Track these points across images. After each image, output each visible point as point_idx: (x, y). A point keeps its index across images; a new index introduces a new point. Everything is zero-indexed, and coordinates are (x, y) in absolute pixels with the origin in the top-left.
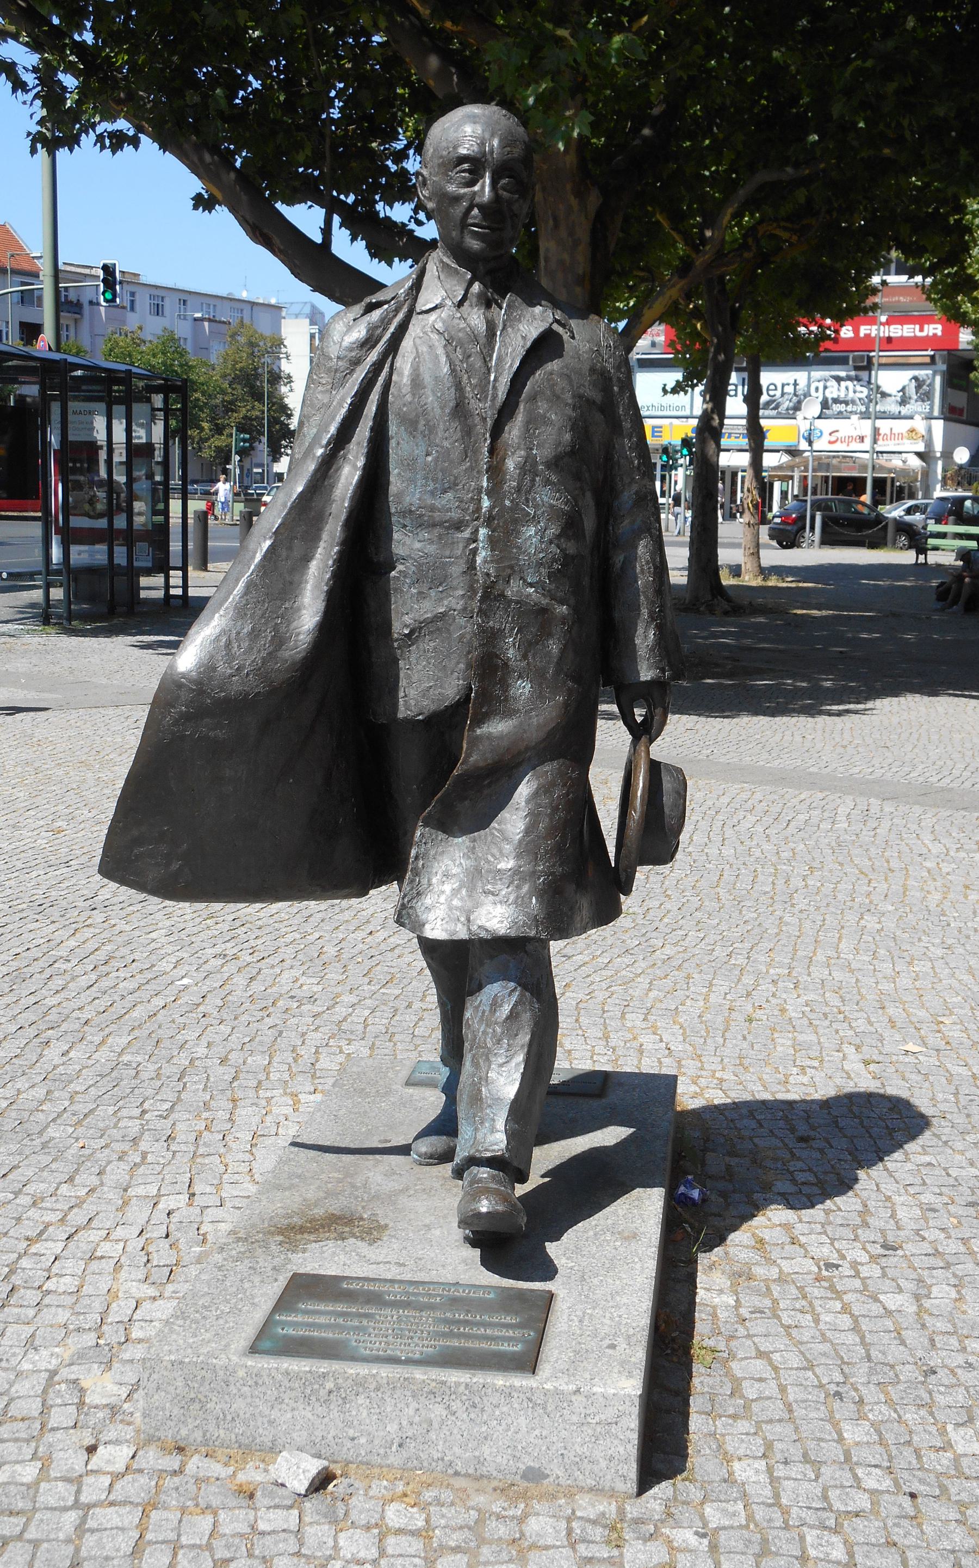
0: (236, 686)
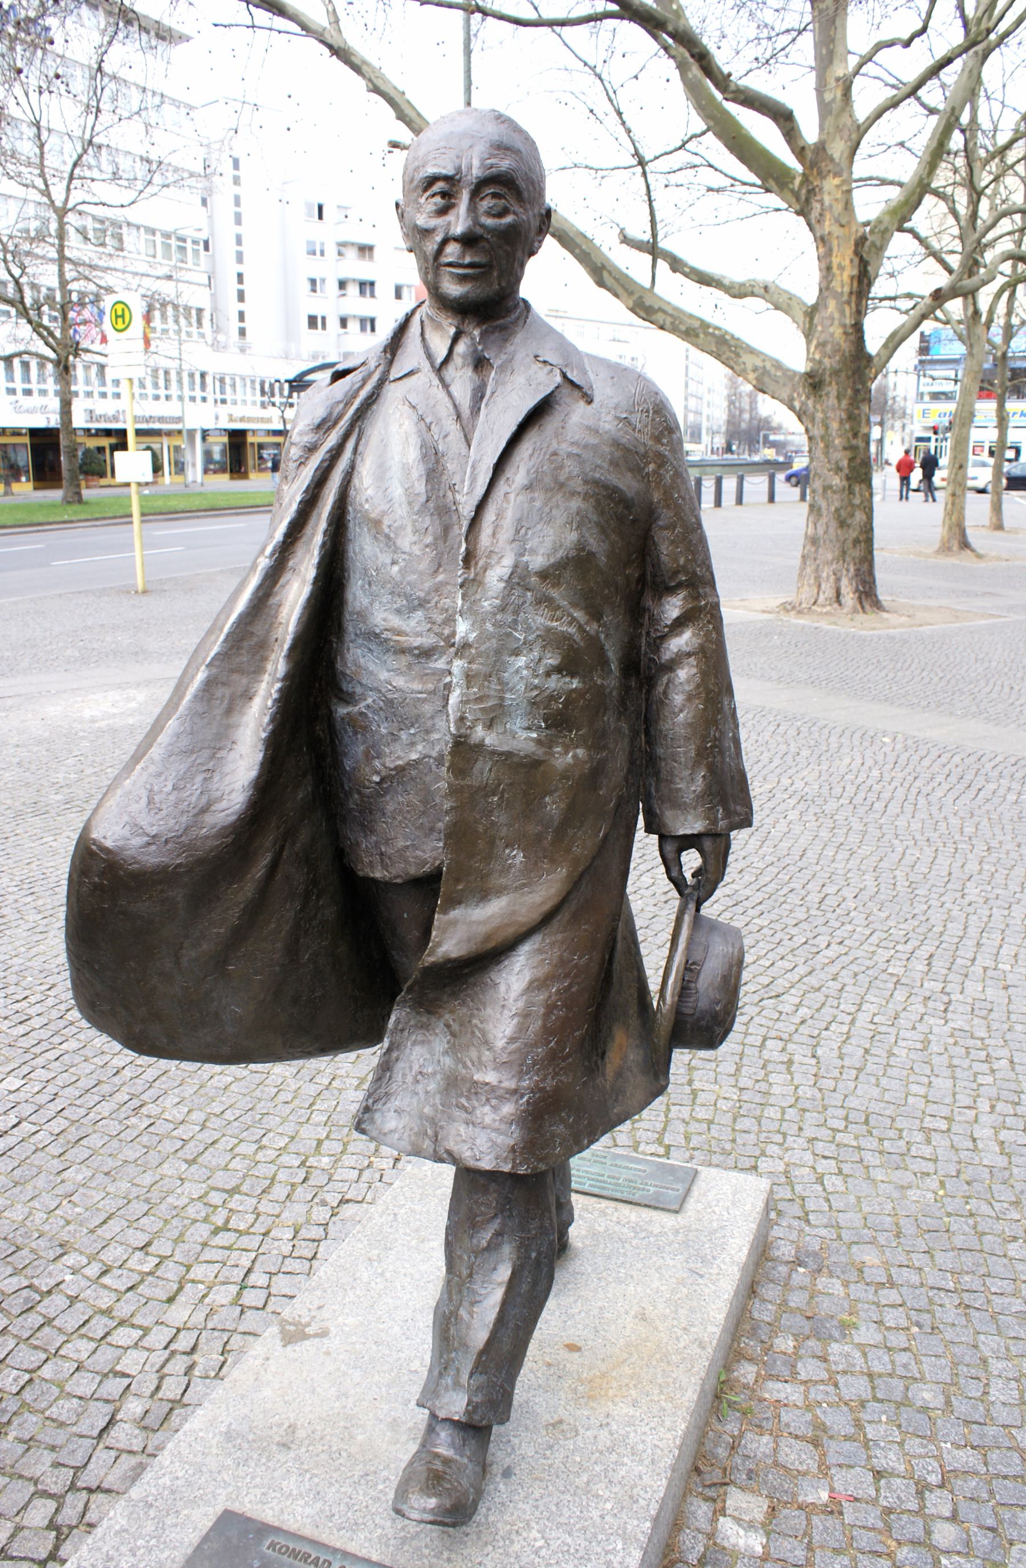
0: (153, 858)
